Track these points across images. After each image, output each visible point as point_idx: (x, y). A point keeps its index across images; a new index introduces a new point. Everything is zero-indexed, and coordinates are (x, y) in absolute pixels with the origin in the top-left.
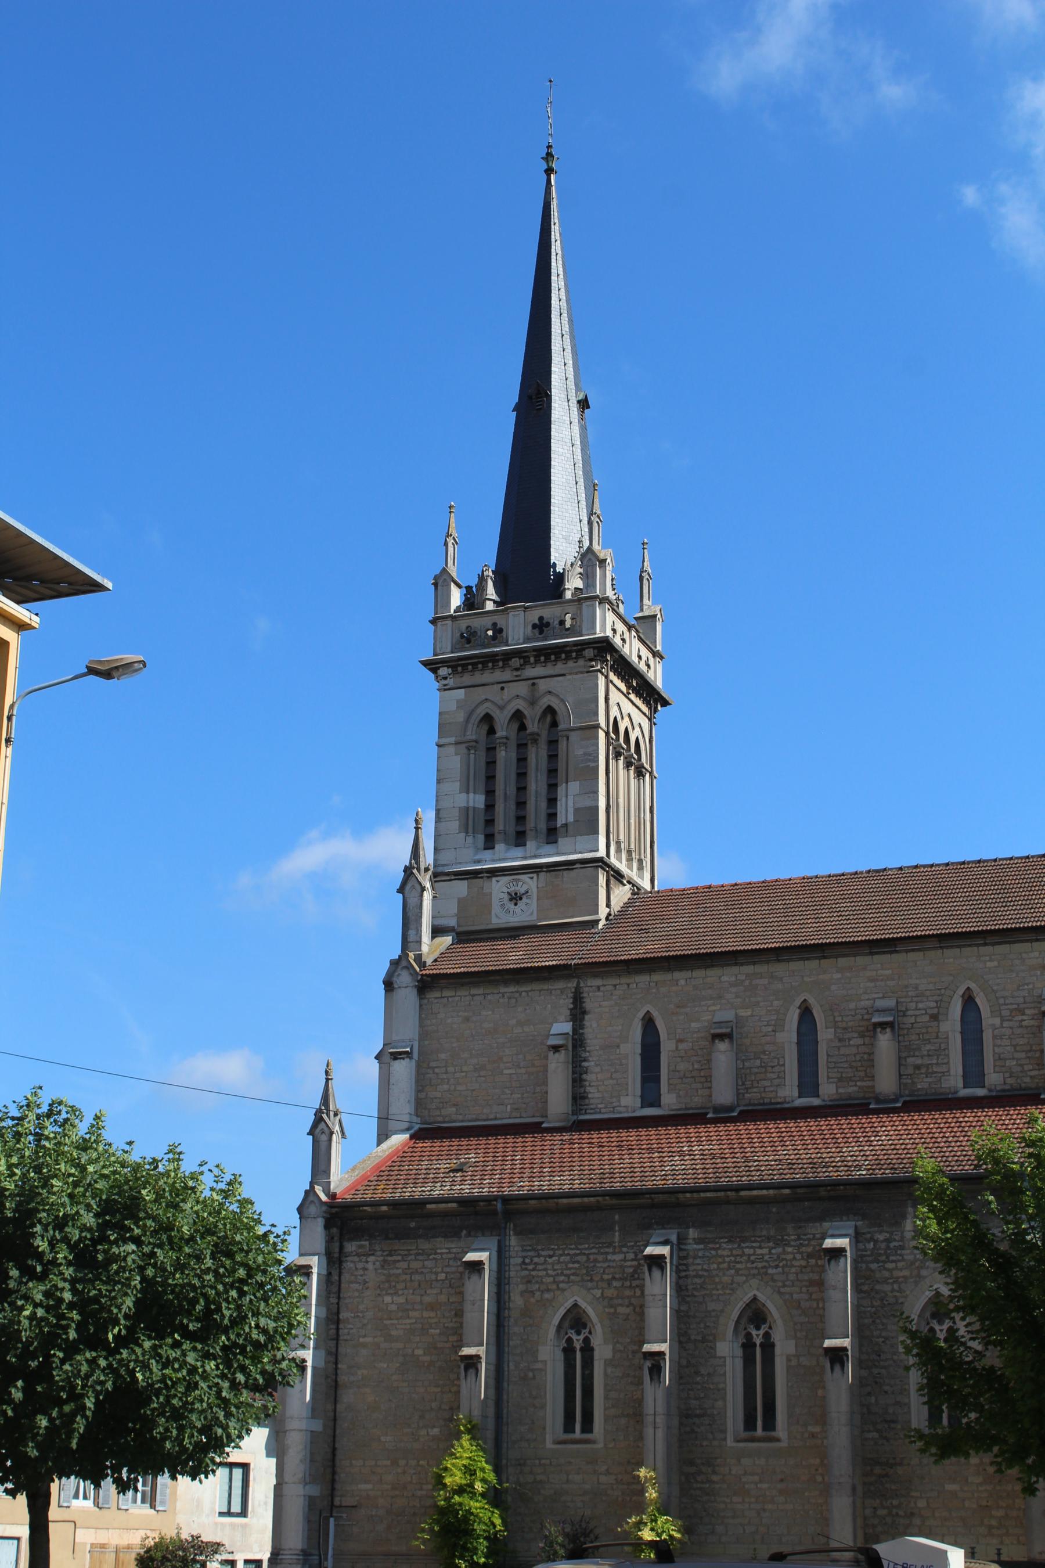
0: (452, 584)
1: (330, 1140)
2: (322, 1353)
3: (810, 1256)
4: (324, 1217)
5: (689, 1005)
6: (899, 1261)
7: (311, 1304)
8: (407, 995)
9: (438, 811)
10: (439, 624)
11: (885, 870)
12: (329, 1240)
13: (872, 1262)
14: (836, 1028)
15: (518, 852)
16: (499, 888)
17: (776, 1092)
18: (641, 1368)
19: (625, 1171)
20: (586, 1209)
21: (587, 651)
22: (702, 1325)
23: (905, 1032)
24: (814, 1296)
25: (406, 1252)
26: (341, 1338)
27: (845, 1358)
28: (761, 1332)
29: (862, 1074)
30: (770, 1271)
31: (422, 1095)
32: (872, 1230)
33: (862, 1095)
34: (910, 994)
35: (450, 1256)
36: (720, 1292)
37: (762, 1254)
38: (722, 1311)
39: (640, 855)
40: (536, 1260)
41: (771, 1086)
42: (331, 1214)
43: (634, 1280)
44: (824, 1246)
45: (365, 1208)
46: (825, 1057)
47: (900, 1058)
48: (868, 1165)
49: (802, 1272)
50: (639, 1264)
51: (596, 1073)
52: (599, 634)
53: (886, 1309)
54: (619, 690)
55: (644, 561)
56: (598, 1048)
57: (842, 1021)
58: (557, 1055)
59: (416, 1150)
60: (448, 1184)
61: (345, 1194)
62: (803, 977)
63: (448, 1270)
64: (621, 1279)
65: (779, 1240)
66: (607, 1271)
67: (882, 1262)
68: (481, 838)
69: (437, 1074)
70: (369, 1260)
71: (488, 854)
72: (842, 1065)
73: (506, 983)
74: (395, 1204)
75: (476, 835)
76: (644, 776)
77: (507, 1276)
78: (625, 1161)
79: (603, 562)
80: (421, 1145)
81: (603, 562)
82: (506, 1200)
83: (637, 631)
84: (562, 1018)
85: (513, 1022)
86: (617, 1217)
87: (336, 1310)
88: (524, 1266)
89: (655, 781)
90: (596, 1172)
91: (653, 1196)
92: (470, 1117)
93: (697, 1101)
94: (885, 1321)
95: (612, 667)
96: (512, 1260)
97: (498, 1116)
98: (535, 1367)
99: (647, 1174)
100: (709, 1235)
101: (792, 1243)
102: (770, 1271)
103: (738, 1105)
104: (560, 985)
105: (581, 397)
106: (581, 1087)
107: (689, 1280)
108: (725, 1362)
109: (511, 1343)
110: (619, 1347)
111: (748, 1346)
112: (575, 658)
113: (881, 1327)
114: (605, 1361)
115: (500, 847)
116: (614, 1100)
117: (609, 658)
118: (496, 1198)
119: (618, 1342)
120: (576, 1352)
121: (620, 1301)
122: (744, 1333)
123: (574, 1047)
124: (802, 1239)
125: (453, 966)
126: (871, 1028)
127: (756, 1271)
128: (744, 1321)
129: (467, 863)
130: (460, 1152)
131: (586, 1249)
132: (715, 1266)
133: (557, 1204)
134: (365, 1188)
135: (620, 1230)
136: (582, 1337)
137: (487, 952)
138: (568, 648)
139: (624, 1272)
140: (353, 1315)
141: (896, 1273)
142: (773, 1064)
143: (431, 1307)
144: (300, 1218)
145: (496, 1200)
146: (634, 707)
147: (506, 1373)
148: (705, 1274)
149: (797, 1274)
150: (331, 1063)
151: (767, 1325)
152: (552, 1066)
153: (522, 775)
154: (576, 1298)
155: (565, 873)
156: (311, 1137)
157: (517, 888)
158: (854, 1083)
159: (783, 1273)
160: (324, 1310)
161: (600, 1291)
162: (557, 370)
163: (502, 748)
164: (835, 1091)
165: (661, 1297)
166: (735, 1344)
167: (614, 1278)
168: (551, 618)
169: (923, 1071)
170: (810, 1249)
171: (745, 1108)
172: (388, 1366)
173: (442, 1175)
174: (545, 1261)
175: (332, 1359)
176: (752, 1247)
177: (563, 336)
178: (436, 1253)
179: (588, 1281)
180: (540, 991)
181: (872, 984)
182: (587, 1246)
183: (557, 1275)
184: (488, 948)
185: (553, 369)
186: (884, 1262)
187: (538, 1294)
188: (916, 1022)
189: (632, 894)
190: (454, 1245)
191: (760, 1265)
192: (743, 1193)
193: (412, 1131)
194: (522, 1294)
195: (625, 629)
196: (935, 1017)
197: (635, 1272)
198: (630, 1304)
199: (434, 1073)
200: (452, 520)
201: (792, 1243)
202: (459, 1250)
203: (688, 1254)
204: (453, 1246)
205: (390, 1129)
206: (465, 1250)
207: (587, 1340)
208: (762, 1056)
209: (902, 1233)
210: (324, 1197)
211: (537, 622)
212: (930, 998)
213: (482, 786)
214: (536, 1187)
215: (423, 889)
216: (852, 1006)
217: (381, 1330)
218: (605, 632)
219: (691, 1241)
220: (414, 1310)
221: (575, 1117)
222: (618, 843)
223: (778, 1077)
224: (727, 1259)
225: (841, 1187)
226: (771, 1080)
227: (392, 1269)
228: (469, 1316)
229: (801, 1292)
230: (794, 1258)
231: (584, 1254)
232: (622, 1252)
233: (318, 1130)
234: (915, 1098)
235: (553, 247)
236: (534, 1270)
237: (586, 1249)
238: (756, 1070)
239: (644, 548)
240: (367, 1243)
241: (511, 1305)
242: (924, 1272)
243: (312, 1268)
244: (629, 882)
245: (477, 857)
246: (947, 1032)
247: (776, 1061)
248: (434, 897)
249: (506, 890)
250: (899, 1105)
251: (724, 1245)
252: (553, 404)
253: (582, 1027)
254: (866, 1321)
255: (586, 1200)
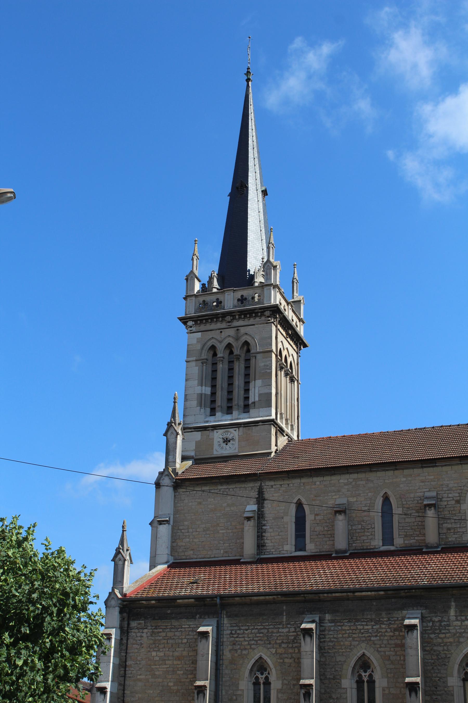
0: (196, 279)
1: (124, 564)
2: (116, 684)
3: (395, 630)
4: (119, 607)
5: (322, 495)
6: (447, 633)
7: (111, 656)
8: (168, 491)
9: (186, 395)
10: (188, 299)
11: (425, 428)
12: (122, 620)
13: (431, 634)
14: (403, 508)
15: (229, 417)
16: (218, 435)
17: (370, 543)
18: (298, 694)
19: (289, 582)
20: (267, 603)
21: (266, 312)
22: (333, 670)
23: (442, 510)
24: (398, 653)
25: (165, 627)
26: (127, 676)
27: (418, 689)
28: (367, 674)
29: (418, 533)
30: (372, 639)
31: (174, 544)
32: (432, 615)
33: (418, 544)
34: (444, 489)
35: (189, 629)
36: (344, 650)
37: (367, 629)
38: (345, 661)
39: (292, 423)
40: (238, 632)
41: (367, 539)
42: (123, 605)
43: (294, 643)
44: (405, 624)
45: (142, 602)
46: (397, 524)
47: (439, 524)
48: (427, 579)
49: (391, 639)
50: (297, 634)
51: (271, 532)
52: (273, 302)
53: (440, 661)
54: (282, 334)
55: (294, 274)
56: (271, 519)
57: (407, 504)
58: (249, 522)
59: (171, 573)
60: (189, 589)
61: (131, 594)
62: (384, 480)
63: (188, 637)
64: (287, 643)
65: (377, 621)
66: (279, 638)
67: (437, 633)
68: (208, 410)
69: (183, 533)
70: (144, 631)
71: (212, 418)
72: (406, 528)
73: (221, 484)
74: (159, 599)
75: (206, 408)
76: (294, 382)
77: (222, 641)
78: (288, 578)
79: (275, 267)
80: (174, 571)
81: (275, 267)
82: (222, 597)
83: (292, 306)
84: (252, 502)
85: (225, 505)
86: (285, 607)
87: (124, 660)
88: (231, 635)
89: (299, 385)
90: (272, 583)
91: (306, 595)
92: (200, 556)
93: (326, 548)
94: (439, 668)
95: (279, 321)
96: (224, 632)
97: (216, 556)
98: (238, 693)
99: (301, 584)
100: (337, 618)
101: (385, 623)
102: (372, 639)
103: (349, 550)
104: (251, 485)
105: (263, 189)
106: (262, 540)
107: (326, 644)
108: (347, 691)
109: (224, 679)
110: (286, 682)
111: (360, 682)
112: (260, 316)
113: (437, 671)
114: (278, 690)
115: (218, 414)
116: (280, 547)
117: (278, 317)
118: (216, 596)
119: (285, 679)
120: (260, 684)
121: (286, 655)
122: (357, 674)
123: (259, 518)
124: (391, 620)
125: (193, 475)
126: (423, 508)
127: (364, 639)
128: (357, 667)
129: (201, 422)
130: (195, 574)
131: (267, 626)
132: (341, 635)
133: (251, 600)
134: (142, 592)
135: (286, 615)
136: (264, 676)
137: (211, 468)
138: (256, 311)
139: (288, 639)
140: (134, 663)
141: (445, 640)
142: (368, 528)
143: (178, 658)
144: (106, 608)
145: (216, 597)
146: (289, 345)
147: (220, 697)
148: (335, 640)
149: (388, 640)
150: (126, 522)
151: (371, 670)
152: (246, 528)
153: (231, 377)
154: (261, 653)
155: (254, 427)
156: (113, 562)
157: (227, 436)
158: (413, 538)
159: (380, 640)
160: (118, 659)
161: (275, 650)
162: (251, 175)
163: (221, 363)
164: (403, 543)
165: (310, 653)
166: (352, 681)
167: (283, 642)
168: (247, 296)
169: (452, 531)
170: (395, 626)
171: (353, 551)
172: (153, 692)
173: (186, 585)
174: (244, 632)
175: (122, 688)
176: (362, 625)
177: (254, 159)
178: (182, 628)
179: (268, 644)
180: (240, 488)
181: (423, 484)
182: (267, 624)
183: (250, 640)
184: (212, 466)
185: (249, 174)
186: (439, 634)
187: (239, 651)
188: (448, 504)
189: (288, 441)
190: (192, 623)
191: (367, 635)
192: (357, 594)
193: (169, 564)
194: (230, 651)
195: (286, 304)
196: (458, 502)
197: (295, 638)
198: (292, 657)
199: (181, 532)
200: (196, 247)
201: (385, 623)
202: (195, 626)
203: (325, 629)
204: (192, 624)
205: (156, 562)
206: (198, 626)
207: (267, 678)
208: (362, 523)
209: (449, 617)
210: (119, 596)
211: (240, 298)
212: (455, 492)
213: (209, 383)
214: (239, 591)
215: (177, 434)
216: (412, 495)
217: (149, 671)
218: (276, 302)
219: (327, 621)
220: (169, 660)
221: (258, 557)
222: (281, 414)
223: (371, 535)
224: (348, 632)
225: (413, 590)
226: (367, 536)
227: (157, 636)
228: (200, 663)
229: (390, 651)
230: (386, 631)
231: (266, 628)
232: (287, 627)
233: (117, 559)
234: (448, 546)
235: (250, 116)
236: (237, 637)
237: (267, 626)
238: (359, 531)
239: (294, 267)
240: (143, 622)
241: (224, 657)
242: (462, 640)
243: (111, 635)
244: (287, 435)
245: (206, 419)
246: (465, 510)
247: (370, 526)
248: (183, 439)
249: (221, 437)
250: (439, 549)
251: (346, 624)
252: (249, 191)
253: (263, 507)
254: (429, 668)
255: (267, 597)
